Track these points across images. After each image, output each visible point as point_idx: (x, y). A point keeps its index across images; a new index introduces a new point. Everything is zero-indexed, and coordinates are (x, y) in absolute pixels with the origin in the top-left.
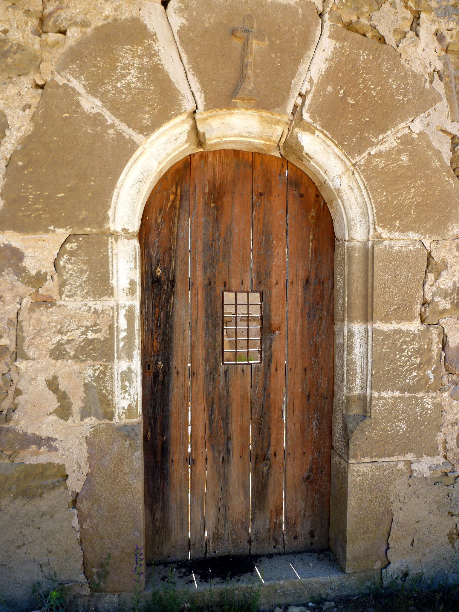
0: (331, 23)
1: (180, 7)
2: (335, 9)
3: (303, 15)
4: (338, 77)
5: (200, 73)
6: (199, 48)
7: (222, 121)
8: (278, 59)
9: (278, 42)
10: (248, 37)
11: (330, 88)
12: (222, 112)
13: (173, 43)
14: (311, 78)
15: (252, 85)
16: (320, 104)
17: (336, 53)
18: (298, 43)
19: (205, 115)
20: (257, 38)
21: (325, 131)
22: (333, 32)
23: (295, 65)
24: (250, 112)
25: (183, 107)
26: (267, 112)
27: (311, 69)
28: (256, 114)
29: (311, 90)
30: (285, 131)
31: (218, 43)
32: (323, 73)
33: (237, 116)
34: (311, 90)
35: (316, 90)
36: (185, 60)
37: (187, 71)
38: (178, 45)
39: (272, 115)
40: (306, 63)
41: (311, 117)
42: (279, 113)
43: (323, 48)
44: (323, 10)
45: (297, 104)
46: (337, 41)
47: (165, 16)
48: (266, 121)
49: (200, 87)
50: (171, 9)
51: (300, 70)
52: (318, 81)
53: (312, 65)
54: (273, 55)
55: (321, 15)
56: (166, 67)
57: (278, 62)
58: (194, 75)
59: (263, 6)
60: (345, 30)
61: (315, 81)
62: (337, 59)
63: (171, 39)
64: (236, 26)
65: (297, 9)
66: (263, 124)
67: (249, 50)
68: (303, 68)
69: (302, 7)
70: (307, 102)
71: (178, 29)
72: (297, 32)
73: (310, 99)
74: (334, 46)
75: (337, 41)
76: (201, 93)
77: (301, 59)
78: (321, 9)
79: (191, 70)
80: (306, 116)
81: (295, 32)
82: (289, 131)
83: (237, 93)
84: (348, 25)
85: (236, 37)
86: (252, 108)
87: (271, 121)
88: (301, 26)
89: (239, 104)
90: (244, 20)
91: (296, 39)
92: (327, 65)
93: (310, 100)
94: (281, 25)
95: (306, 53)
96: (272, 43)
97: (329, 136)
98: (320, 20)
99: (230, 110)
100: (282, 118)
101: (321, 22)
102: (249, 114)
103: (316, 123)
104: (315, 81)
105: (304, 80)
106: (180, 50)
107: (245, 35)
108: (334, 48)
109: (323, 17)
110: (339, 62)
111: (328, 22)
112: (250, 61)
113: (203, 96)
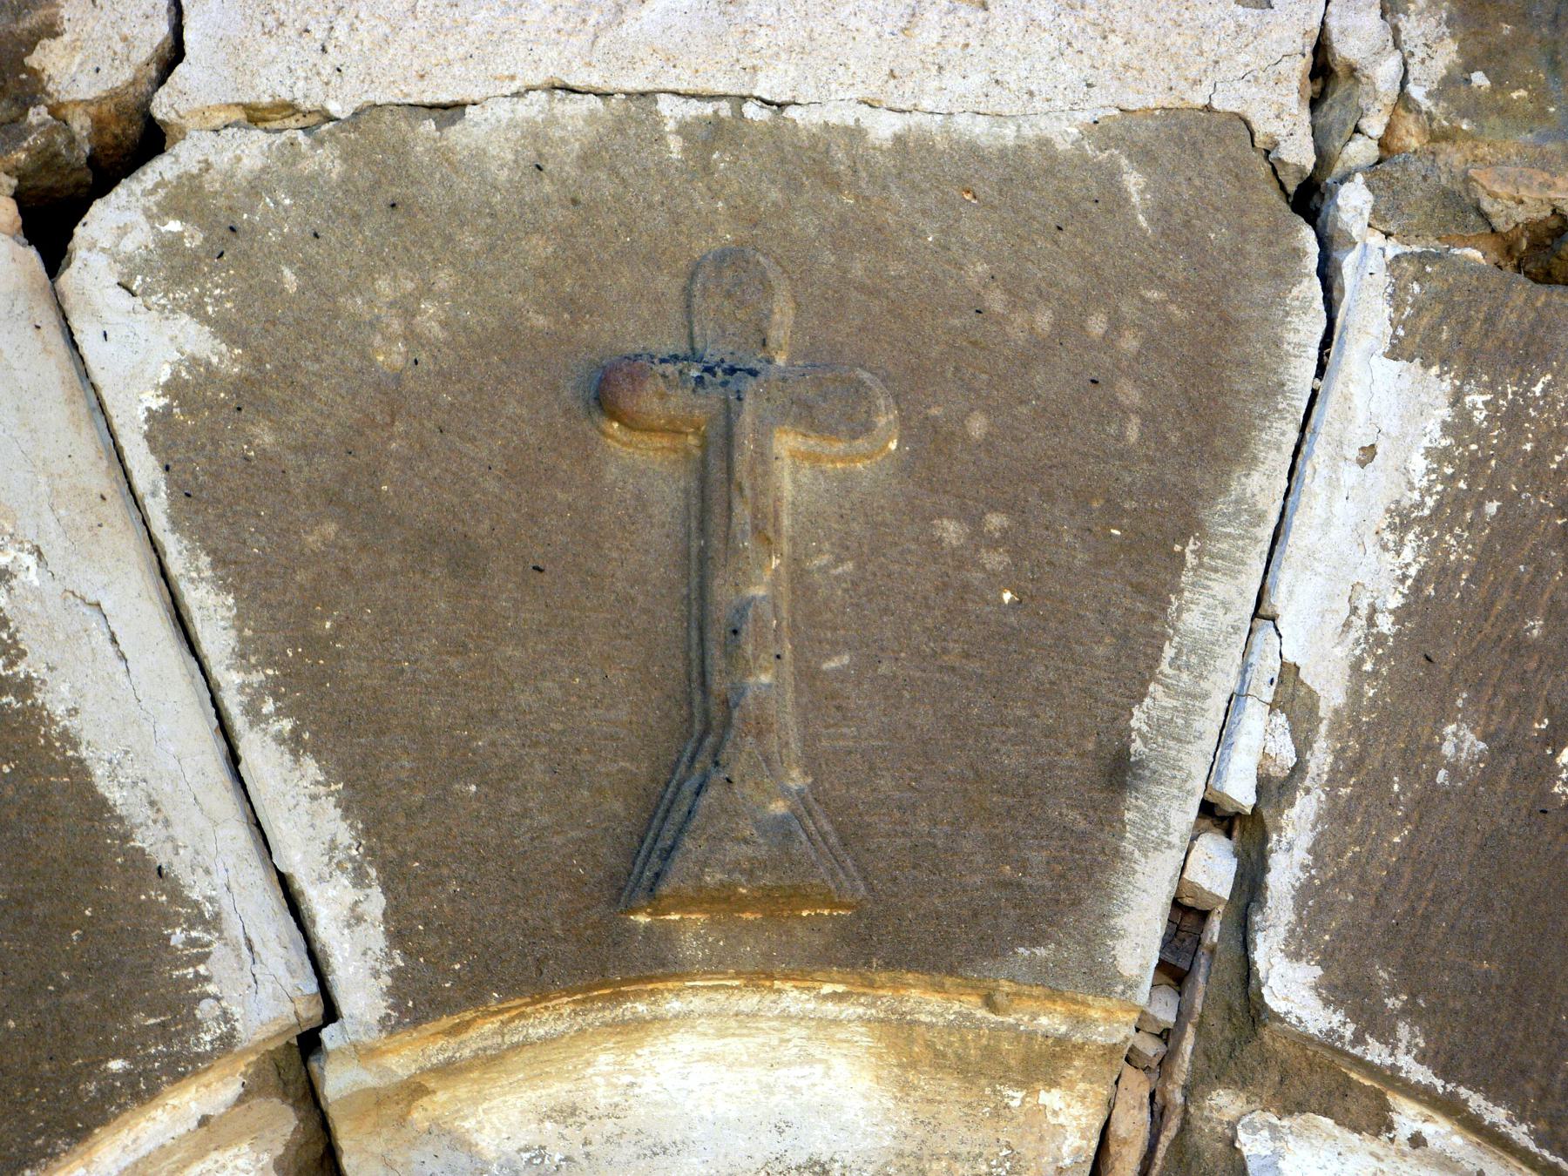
0: (1393, 248)
1: (170, 246)
2: (1411, 137)
3: (1162, 211)
4: (1519, 646)
5: (337, 726)
6: (331, 528)
7: (557, 1091)
8: (995, 560)
9: (977, 426)
10: (729, 417)
11: (1460, 741)
12: (550, 1020)
13: (117, 510)
14: (1289, 673)
15: (797, 779)
16: (1395, 874)
17: (1471, 464)
18: (1148, 418)
19: (403, 1059)
20: (806, 416)
21: (1476, 1102)
22: (1419, 310)
23: (1139, 589)
24: (793, 998)
25: (205, 1009)
26: (939, 988)
27: (1279, 601)
28: (849, 1010)
29: (1299, 768)
30: (1121, 1128)
31: (492, 485)
32: (1385, 624)
33: (684, 1042)
34: (1299, 768)
35: (1347, 766)
36: (216, 639)
37: (239, 722)
38: (159, 523)
39: (990, 1003)
40: (1234, 566)
41: (1332, 992)
42: (1051, 984)
43: (1359, 436)
44: (1324, 159)
45: (1196, 889)
46: (1468, 374)
47: (49, 319)
48: (938, 1060)
49: (345, 836)
50: (99, 262)
51: (1192, 620)
52: (1355, 693)
53: (1284, 577)
54: (951, 531)
55: (1309, 199)
56: (56, 699)
57: (997, 581)
58: (294, 744)
59: (833, 182)
60: (1522, 288)
61: (1331, 693)
62: (1492, 508)
63: (99, 479)
64: (631, 348)
65: (1111, 176)
66: (922, 1082)
67: (743, 513)
68: (1209, 606)
69: (1145, 157)
70: (1285, 873)
71: (158, 403)
72: (1130, 343)
73: (1305, 840)
74: (1445, 413)
75: (1468, 374)
76: (360, 879)
77: (1184, 537)
78: (1299, 153)
79: (268, 707)
80: (1291, 988)
81: (1108, 341)
82: (1158, 1114)
83: (667, 854)
84: (1535, 245)
85: (631, 423)
86: (808, 964)
87: (990, 1053)
88: (1154, 295)
89: (690, 947)
90: (687, 292)
91: (1129, 393)
92: (1411, 556)
93: (1301, 855)
94: (996, 301)
95: (1225, 490)
96: (930, 440)
97: (1520, 1134)
98: (1307, 237)
99: (617, 998)
100: (1079, 1021)
101: (1313, 249)
102: (786, 1017)
103: (1387, 1037)
104: (1331, 693)
105: (1235, 701)
106: (175, 565)
107: (707, 404)
108: (1446, 428)
109: (1327, 210)
110: (1509, 531)
111: (1376, 239)
112: (759, 591)
113: (376, 902)
